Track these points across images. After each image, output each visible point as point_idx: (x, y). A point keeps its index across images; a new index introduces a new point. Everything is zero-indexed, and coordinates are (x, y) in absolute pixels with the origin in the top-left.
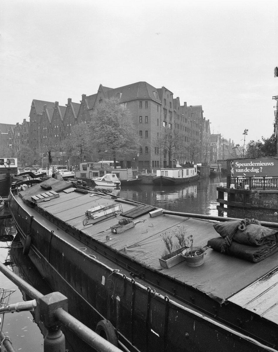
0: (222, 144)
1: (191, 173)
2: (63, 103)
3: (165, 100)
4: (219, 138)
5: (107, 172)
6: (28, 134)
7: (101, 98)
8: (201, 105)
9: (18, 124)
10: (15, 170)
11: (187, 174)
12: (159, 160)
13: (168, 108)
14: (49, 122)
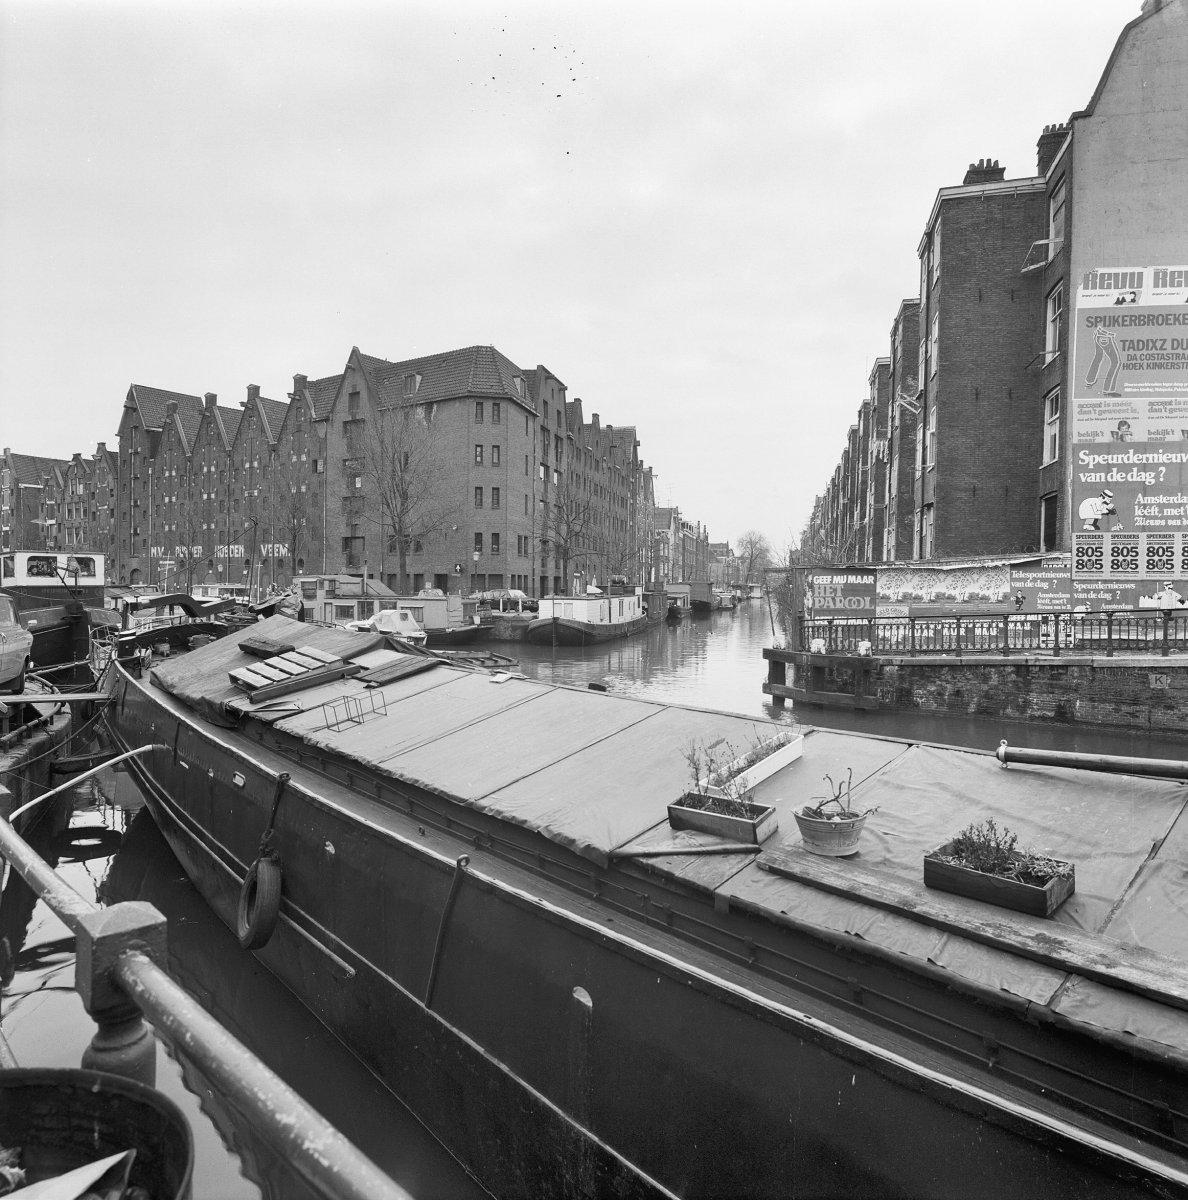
0: (681, 535)
1: (628, 610)
2: (232, 399)
3: (545, 403)
4: (675, 518)
5: (383, 607)
6: (112, 490)
7: (354, 387)
8: (632, 425)
9: (77, 457)
10: (94, 595)
11: (621, 613)
12: (529, 573)
13: (552, 427)
14: (184, 453)
